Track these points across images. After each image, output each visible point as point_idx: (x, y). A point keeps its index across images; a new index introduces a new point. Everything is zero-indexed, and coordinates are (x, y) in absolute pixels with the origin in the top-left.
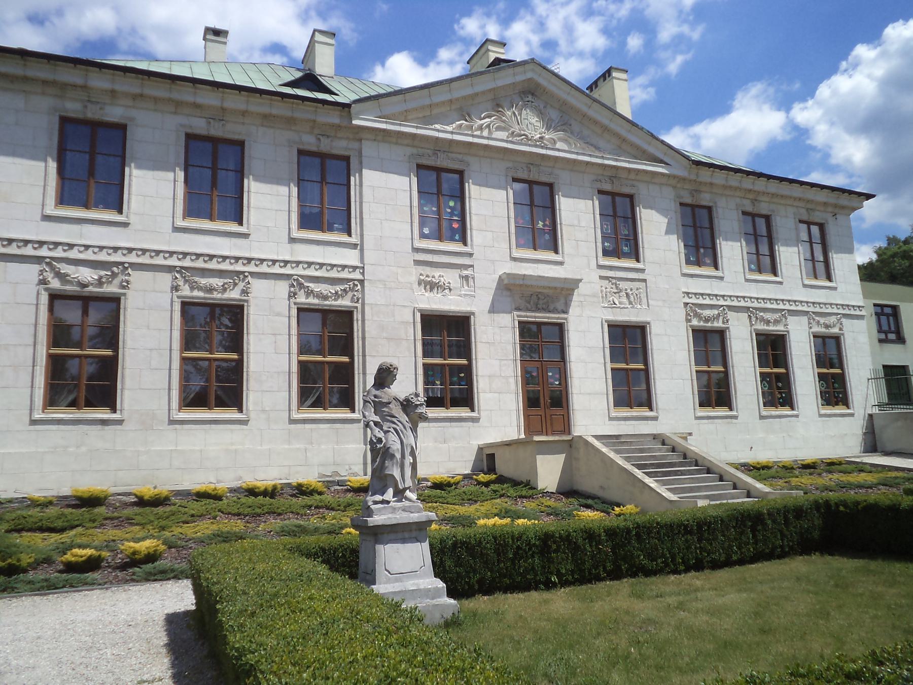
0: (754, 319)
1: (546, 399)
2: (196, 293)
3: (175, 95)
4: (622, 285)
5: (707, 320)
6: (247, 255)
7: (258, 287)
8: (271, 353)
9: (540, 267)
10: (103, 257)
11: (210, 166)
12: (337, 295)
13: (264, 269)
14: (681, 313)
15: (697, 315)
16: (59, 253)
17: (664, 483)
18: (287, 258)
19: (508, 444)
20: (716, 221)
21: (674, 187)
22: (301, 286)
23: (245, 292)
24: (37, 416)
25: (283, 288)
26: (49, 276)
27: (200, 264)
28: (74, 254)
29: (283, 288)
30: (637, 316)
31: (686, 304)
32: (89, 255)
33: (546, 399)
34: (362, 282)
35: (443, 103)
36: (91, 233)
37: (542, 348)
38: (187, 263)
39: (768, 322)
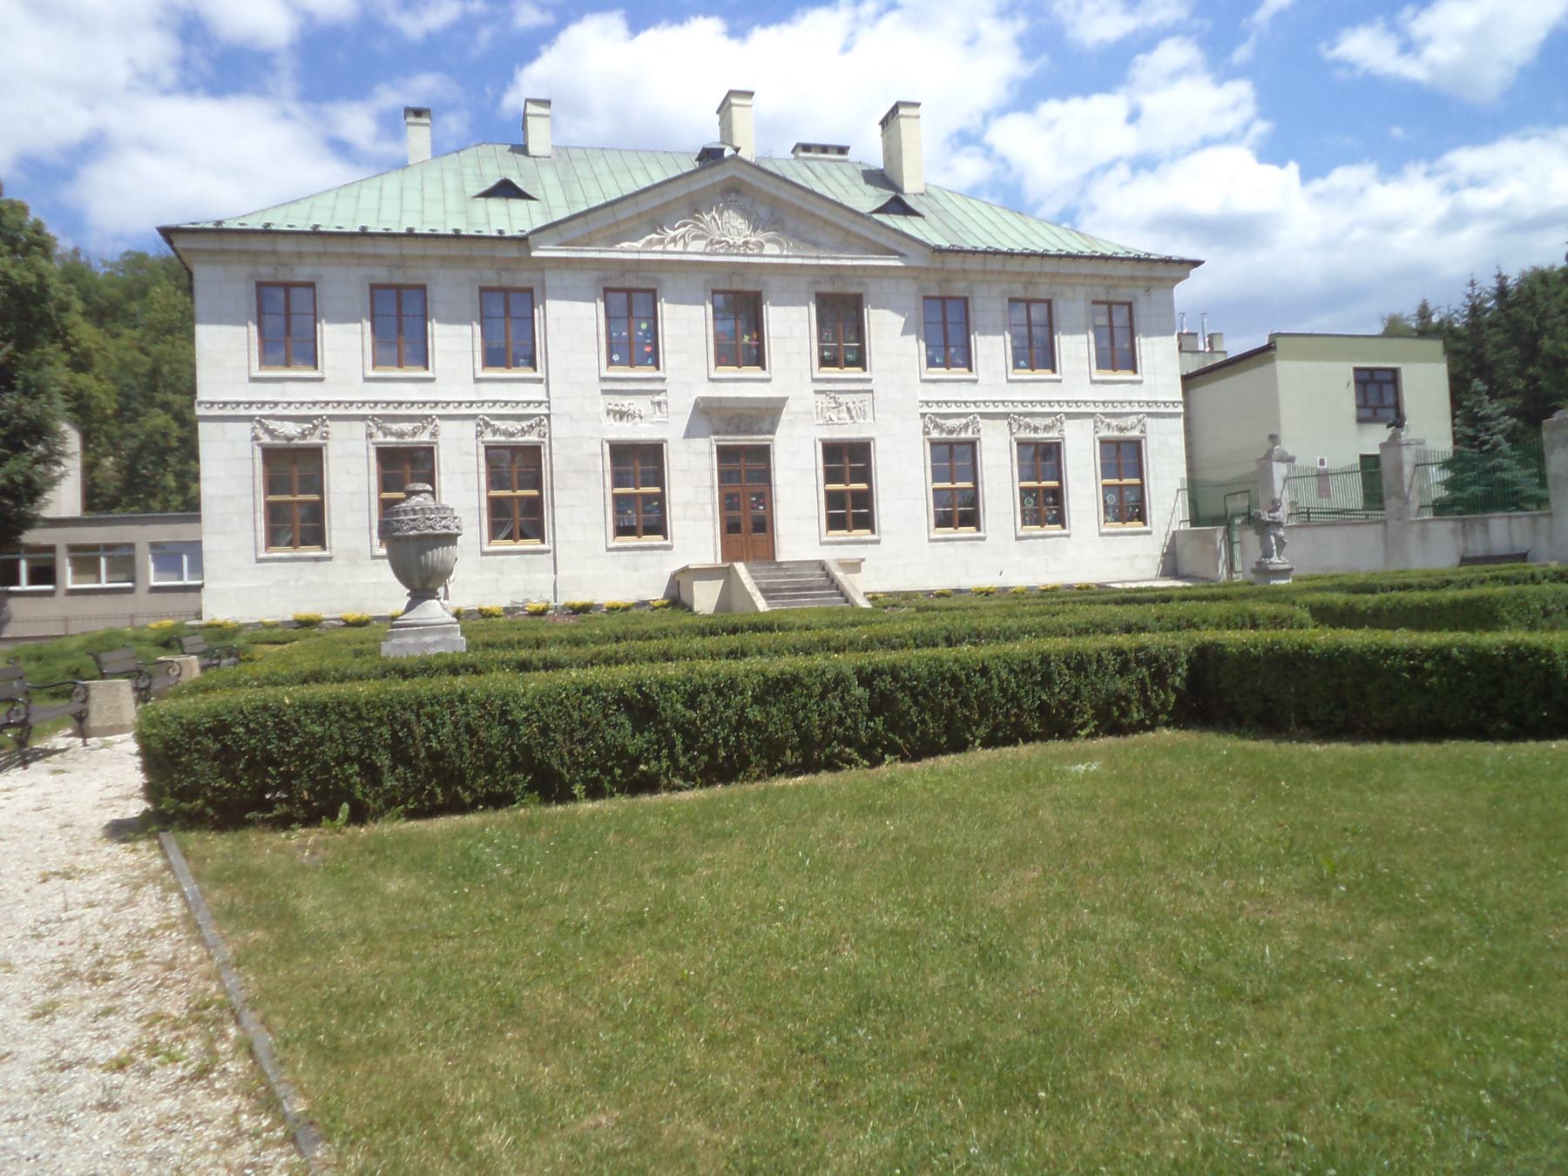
3: (356, 250)
4: (842, 398)
5: (951, 432)
9: (742, 385)
12: (523, 432)
13: (451, 410)
15: (936, 426)
21: (915, 279)
23: (433, 434)
26: (260, 432)
27: (391, 411)
28: (279, 411)
29: (470, 428)
31: (923, 415)
32: (292, 411)
34: (548, 416)
39: (1036, 429)
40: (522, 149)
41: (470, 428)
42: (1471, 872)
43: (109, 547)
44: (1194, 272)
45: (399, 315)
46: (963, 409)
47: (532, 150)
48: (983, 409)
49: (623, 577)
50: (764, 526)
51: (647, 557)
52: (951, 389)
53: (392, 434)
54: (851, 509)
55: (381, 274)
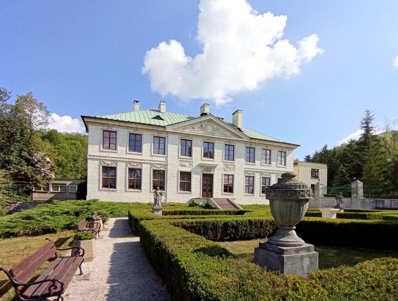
0: (262, 174)
1: (208, 189)
2: (106, 165)
3: (127, 125)
5: (250, 174)
6: (142, 159)
7: (144, 165)
8: (122, 176)
10: (113, 159)
11: (111, 138)
13: (146, 162)
14: (243, 172)
15: (247, 173)
16: (104, 158)
17: (220, 206)
18: (151, 159)
19: (196, 199)
20: (255, 152)
21: (245, 143)
22: (153, 165)
23: (142, 166)
24: (101, 189)
25: (124, 164)
26: (102, 163)
27: (132, 160)
28: (107, 158)
30: (232, 173)
31: (245, 170)
32: (110, 159)
33: (208, 189)
34: (167, 164)
35: (188, 125)
36: (111, 155)
37: (208, 180)
38: (130, 160)
40: (160, 111)
41: (149, 166)
42: (113, 205)
43: (61, 184)
44: (298, 147)
45: (159, 143)
46: (252, 170)
47: (161, 112)
48: (256, 170)
49: (183, 199)
50: (211, 191)
51: (186, 195)
52: (250, 166)
53: (132, 166)
54: (229, 189)
55: (132, 131)
